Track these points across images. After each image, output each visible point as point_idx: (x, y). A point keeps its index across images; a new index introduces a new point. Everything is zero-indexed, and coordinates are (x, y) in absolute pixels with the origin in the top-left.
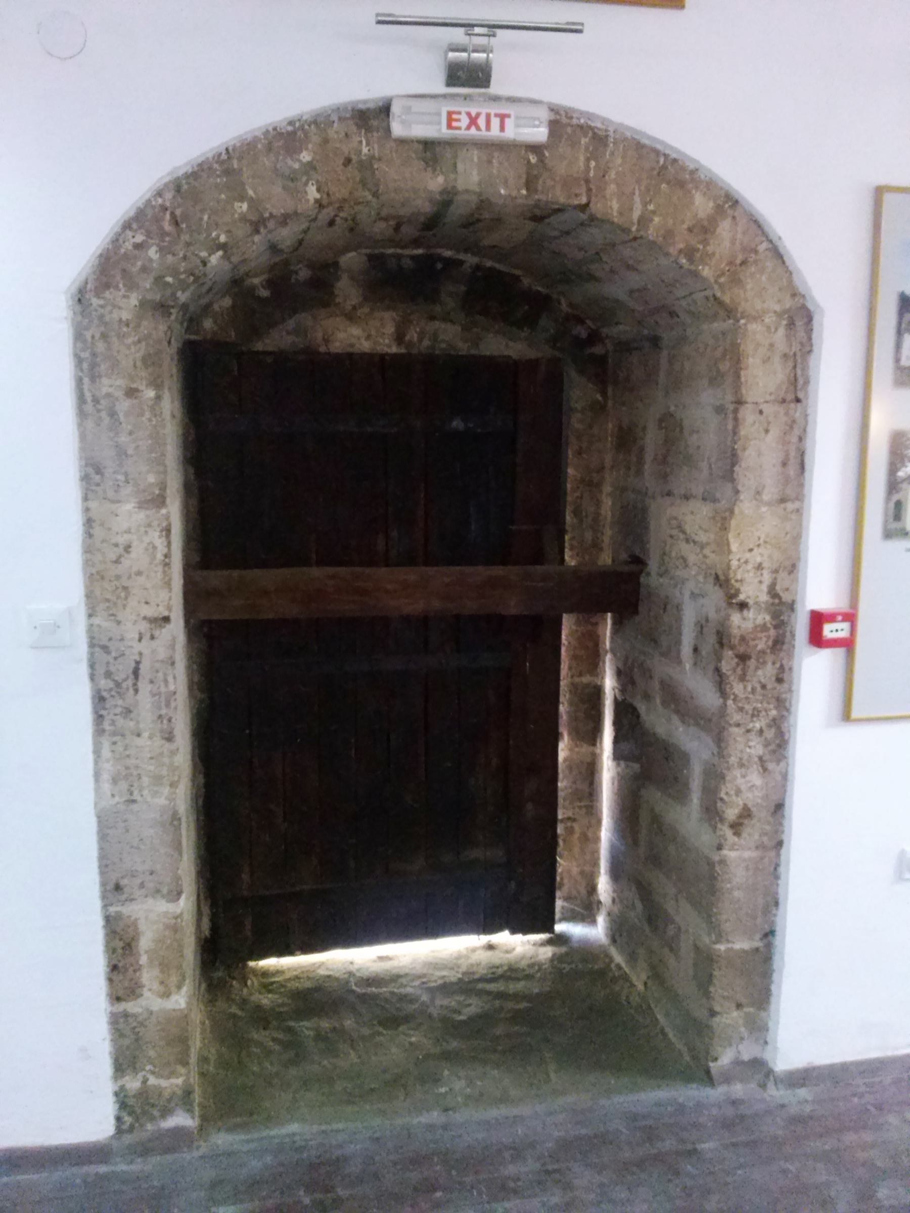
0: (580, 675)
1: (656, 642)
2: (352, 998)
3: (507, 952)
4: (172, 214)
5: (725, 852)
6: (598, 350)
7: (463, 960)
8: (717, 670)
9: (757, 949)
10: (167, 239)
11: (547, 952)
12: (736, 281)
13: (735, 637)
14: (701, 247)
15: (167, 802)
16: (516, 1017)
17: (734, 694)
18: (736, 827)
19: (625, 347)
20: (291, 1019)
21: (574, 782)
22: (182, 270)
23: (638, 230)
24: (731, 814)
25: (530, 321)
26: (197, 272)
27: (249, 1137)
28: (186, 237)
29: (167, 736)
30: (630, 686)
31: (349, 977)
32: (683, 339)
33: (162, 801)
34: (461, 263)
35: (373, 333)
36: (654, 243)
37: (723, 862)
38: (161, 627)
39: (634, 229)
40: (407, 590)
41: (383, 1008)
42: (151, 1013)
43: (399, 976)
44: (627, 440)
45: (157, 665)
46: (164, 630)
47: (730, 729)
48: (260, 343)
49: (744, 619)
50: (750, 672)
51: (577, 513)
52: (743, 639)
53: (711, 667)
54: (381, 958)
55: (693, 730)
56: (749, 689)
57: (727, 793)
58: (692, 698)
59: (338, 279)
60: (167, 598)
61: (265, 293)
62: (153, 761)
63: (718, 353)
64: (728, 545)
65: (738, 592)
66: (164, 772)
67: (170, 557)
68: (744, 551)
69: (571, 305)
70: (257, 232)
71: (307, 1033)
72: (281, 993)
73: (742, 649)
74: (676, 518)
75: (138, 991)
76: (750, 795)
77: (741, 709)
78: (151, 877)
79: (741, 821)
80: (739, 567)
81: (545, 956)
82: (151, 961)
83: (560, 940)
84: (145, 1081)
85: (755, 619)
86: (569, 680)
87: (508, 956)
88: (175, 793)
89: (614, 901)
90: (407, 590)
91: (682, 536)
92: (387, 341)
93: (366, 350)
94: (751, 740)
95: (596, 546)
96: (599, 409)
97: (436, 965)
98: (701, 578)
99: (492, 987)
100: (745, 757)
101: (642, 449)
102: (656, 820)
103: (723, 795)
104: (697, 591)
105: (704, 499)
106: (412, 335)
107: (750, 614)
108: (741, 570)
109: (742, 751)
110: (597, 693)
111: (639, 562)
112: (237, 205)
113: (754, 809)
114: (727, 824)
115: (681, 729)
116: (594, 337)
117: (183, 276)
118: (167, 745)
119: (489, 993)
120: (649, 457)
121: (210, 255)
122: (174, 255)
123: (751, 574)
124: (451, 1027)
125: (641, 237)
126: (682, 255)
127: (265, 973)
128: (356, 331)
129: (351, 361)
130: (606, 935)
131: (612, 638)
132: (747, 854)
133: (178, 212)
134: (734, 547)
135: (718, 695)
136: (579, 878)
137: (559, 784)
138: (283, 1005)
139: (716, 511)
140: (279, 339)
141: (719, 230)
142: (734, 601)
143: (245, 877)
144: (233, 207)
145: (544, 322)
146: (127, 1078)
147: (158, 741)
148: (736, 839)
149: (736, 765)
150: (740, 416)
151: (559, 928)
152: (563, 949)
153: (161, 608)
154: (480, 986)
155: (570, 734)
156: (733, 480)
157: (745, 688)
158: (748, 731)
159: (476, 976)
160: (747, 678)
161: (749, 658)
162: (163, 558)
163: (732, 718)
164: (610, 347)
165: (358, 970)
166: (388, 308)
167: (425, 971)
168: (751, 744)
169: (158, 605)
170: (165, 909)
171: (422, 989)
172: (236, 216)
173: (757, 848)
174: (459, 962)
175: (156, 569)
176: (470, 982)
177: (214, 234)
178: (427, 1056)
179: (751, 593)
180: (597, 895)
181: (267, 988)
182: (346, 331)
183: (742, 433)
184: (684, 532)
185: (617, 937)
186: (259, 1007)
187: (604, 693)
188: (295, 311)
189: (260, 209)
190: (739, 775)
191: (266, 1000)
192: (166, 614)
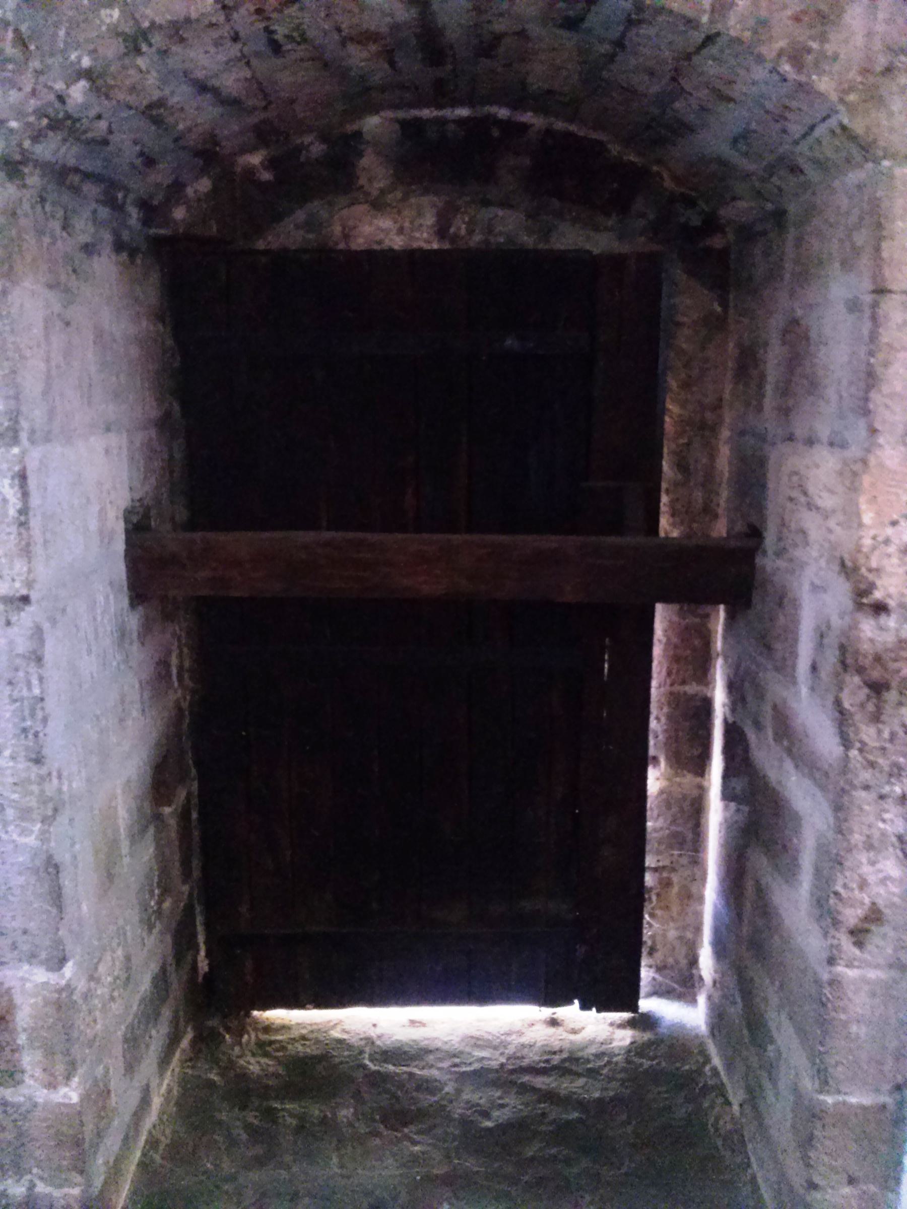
0: (684, 682)
1: (769, 648)
2: (359, 1075)
3: (574, 1032)
4: (16, 31)
5: (840, 969)
6: (717, 242)
7: (514, 1037)
8: (838, 703)
9: (884, 1107)
10: (10, 67)
11: (625, 1038)
12: (874, 98)
13: (865, 656)
14: (815, 45)
15: (39, 843)
16: (562, 1133)
17: (861, 742)
18: (859, 935)
19: (748, 234)
20: (276, 1098)
21: (674, 821)
22: (30, 110)
23: (712, 21)
24: (852, 916)
25: (620, 205)
26: (50, 111)
27: (490, 1062)
28: (35, 64)
29: (34, 756)
30: (740, 704)
31: (366, 1045)
32: (810, 211)
33: (31, 840)
34: (524, 127)
35: (407, 224)
36: (738, 41)
37: (834, 982)
38: (20, 609)
39: (705, 19)
40: (420, 563)
41: (394, 1096)
42: (35, 1105)
43: (427, 1051)
44: (748, 364)
45: (18, 661)
46: (22, 614)
47: (854, 793)
48: (261, 241)
49: (881, 628)
50: (888, 709)
51: (682, 466)
52: (878, 659)
53: (831, 698)
54: (413, 1022)
55: (807, 783)
56: (886, 735)
57: (845, 886)
58: (807, 736)
59: (360, 155)
60: (25, 569)
61: (266, 176)
62: (19, 789)
63: (853, 219)
64: (858, 515)
65: (872, 586)
66: (34, 804)
67: (27, 514)
68: (882, 524)
69: (676, 179)
70: (138, 51)
71: (289, 1120)
72: (276, 1058)
73: (876, 674)
74: (796, 473)
75: (18, 1077)
76: (882, 891)
77: (872, 765)
78: (25, 937)
79: (866, 926)
80: (874, 548)
81: (622, 1044)
82: (30, 1040)
83: (646, 1022)
84: (32, 1187)
85: (897, 630)
86: (668, 688)
87: (572, 1037)
88: (48, 831)
89: (715, 982)
90: (420, 563)
91: (803, 499)
92: (425, 235)
93: (396, 247)
94: (887, 811)
95: (709, 511)
96: (716, 325)
97: (477, 1042)
98: (823, 563)
99: (540, 1082)
100: (876, 835)
101: (762, 377)
102: (761, 892)
103: (839, 888)
104: (817, 582)
105: (831, 444)
106: (459, 226)
107: (891, 622)
108: (877, 553)
109: (870, 826)
110: (707, 705)
111: (756, 533)
112: (104, 12)
113: (887, 911)
114: (843, 930)
115: (794, 778)
116: (712, 225)
117: (32, 119)
118: (35, 768)
119: (534, 1089)
120: (769, 389)
121: (68, 87)
122: (20, 89)
123: (895, 560)
124: (473, 1137)
125: (718, 34)
126: (785, 59)
127: (268, 1028)
128: (385, 223)
129: (377, 259)
130: (706, 1023)
131: (725, 638)
132: (873, 974)
133: (23, 28)
134: (867, 518)
135: (837, 740)
136: (677, 944)
137: (649, 824)
138: (276, 1075)
139: (845, 463)
140: (288, 234)
141: (847, 18)
142: (865, 601)
143: (244, 909)
144: (98, 16)
145: (639, 204)
146: (10, 1181)
147: (22, 765)
148: (857, 952)
149: (860, 845)
150: (880, 312)
151: (646, 1004)
152: (647, 1036)
153: (17, 585)
154: (526, 1078)
155: (668, 759)
156: (866, 412)
157: (879, 732)
158: (882, 797)
159: (525, 1063)
160: (883, 718)
161: (886, 686)
162: (16, 515)
163: (857, 776)
164: (731, 237)
165: (379, 1037)
166: (426, 191)
167: (461, 1048)
168: (887, 816)
169: (13, 580)
170: (44, 979)
171: (451, 1073)
172: (104, 28)
173: (891, 966)
174: (509, 1039)
175: (8, 530)
176: (512, 1072)
177: (73, 57)
178: (429, 1179)
179: (892, 590)
180: (698, 968)
181: (263, 1047)
182: (371, 224)
183: (885, 339)
184: (805, 494)
185: (716, 1033)
186: (243, 1076)
187: (714, 710)
188: (304, 199)
189: (137, 16)
190: (864, 860)
191: (254, 1065)
192: (24, 592)
